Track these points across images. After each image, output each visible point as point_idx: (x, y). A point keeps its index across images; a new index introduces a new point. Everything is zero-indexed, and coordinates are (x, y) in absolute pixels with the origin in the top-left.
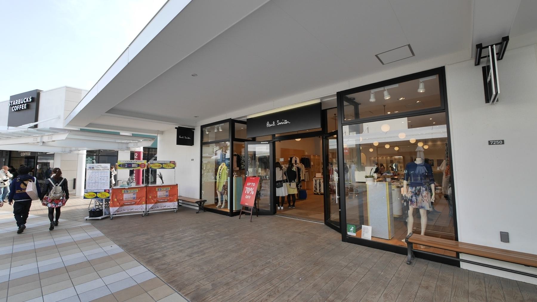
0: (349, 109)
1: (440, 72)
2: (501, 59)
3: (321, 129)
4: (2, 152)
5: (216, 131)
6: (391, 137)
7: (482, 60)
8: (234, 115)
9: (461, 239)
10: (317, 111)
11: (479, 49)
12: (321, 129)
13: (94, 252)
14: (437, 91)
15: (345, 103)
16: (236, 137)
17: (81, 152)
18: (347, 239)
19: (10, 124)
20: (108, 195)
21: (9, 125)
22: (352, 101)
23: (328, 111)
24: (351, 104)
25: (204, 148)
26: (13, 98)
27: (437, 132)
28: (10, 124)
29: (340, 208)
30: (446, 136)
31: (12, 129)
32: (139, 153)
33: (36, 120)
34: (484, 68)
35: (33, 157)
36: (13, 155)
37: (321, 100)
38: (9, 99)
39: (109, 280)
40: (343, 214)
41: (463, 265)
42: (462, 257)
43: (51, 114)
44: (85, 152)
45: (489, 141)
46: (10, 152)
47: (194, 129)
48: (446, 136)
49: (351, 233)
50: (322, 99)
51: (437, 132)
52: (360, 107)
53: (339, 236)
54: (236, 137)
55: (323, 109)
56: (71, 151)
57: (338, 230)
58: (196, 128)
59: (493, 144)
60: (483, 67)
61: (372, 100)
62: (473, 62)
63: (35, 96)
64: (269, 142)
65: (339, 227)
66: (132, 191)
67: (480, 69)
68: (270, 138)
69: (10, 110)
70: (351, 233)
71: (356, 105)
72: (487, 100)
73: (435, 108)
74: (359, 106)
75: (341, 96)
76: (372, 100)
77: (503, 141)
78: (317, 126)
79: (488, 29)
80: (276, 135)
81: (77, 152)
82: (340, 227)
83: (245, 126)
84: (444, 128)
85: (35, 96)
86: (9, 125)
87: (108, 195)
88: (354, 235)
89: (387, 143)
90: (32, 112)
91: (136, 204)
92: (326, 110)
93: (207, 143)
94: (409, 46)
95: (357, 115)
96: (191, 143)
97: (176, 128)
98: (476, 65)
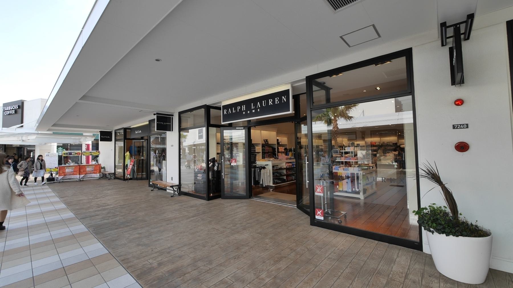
0: (319, 94)
1: (408, 54)
2: (468, 39)
4: (6, 147)
8: (209, 101)
11: (444, 28)
13: (53, 200)
14: (404, 75)
15: (315, 88)
16: (127, 137)
17: (52, 144)
18: (315, 223)
20: (57, 170)
22: (322, 86)
23: (301, 96)
24: (322, 89)
25: (116, 142)
26: (5, 105)
31: (6, 130)
32: (88, 145)
33: (22, 122)
34: (451, 50)
35: (20, 148)
38: (2, 105)
39: (63, 256)
41: (168, 191)
43: (32, 116)
44: (55, 145)
45: (453, 125)
46: (5, 145)
47: (173, 115)
49: (319, 217)
52: (331, 91)
53: (306, 219)
54: (212, 122)
56: (46, 144)
58: (174, 114)
59: (457, 128)
60: (450, 48)
63: (20, 104)
64: (244, 127)
66: (71, 168)
67: (446, 51)
69: (4, 115)
70: (319, 217)
71: (327, 90)
73: (403, 88)
74: (331, 91)
75: (311, 80)
77: (467, 125)
79: (454, 8)
81: (49, 144)
82: (309, 209)
85: (20, 104)
87: (57, 170)
90: (19, 115)
91: (73, 174)
93: (186, 130)
94: (374, 26)
96: (110, 140)
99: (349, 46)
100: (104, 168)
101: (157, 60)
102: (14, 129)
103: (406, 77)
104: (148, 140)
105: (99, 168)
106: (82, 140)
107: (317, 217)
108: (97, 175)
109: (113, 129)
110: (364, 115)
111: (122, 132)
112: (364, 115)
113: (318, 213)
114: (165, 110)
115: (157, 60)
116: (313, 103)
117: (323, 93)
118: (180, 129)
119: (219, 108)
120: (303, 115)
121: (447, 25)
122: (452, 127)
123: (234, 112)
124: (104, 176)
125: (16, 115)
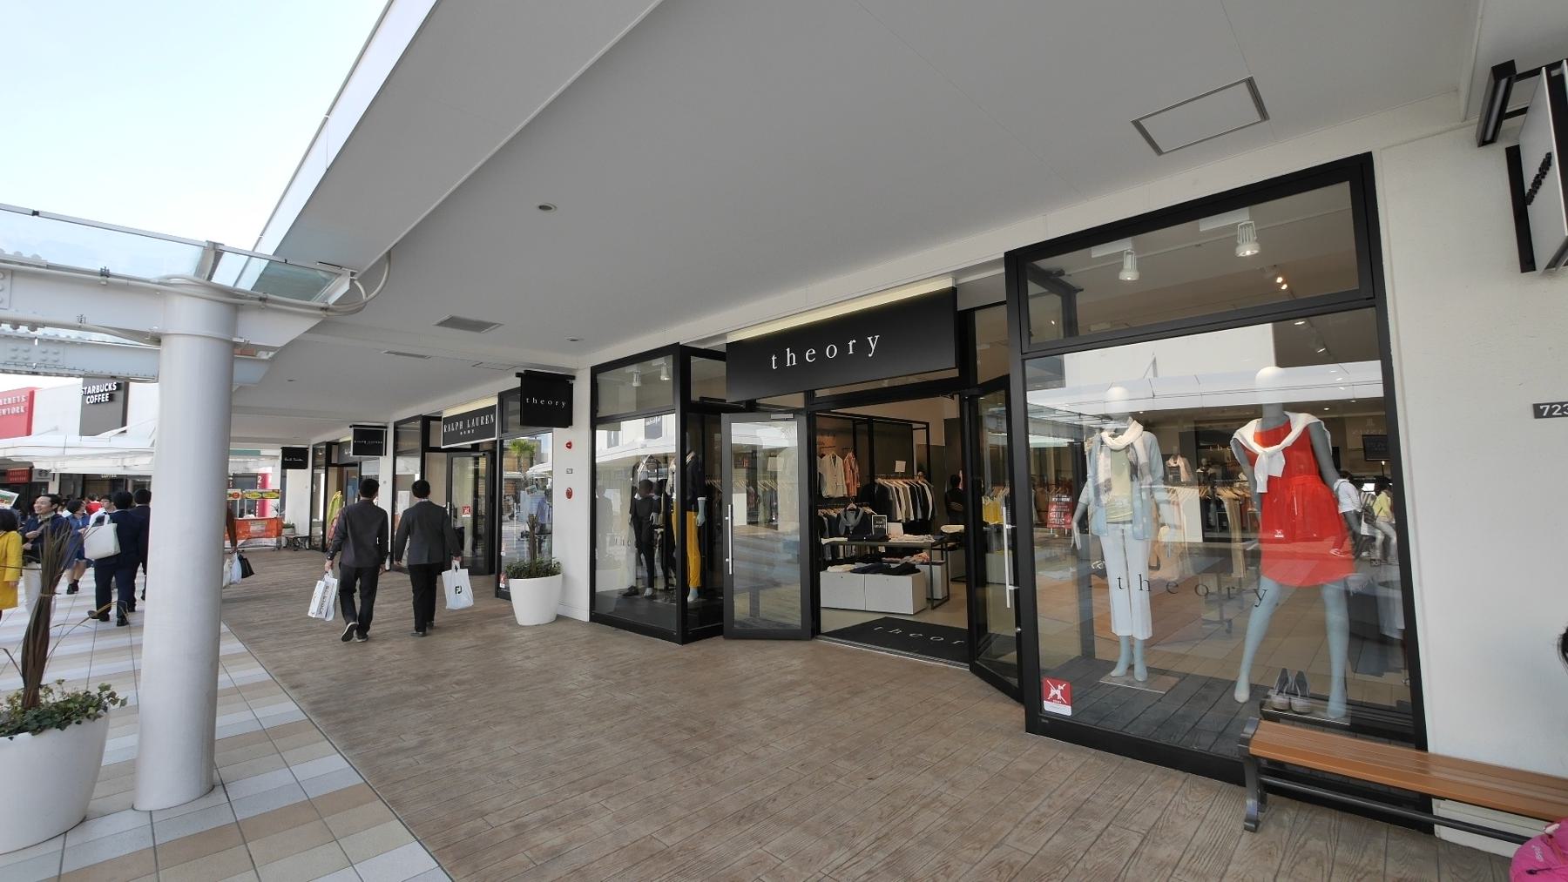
0: (1044, 309)
1: (1357, 173)
3: (955, 373)
5: (635, 384)
6: (1228, 392)
7: (1506, 123)
8: (687, 332)
9: (1435, 743)
10: (945, 315)
12: (955, 373)
15: (1033, 288)
18: (1040, 724)
19: (83, 432)
21: (82, 434)
22: (1054, 281)
23: (978, 314)
24: (1052, 291)
25: (399, 460)
27: (1354, 380)
28: (83, 432)
29: (1018, 624)
30: (1378, 391)
33: (124, 423)
36: (876, 427)
37: (955, 279)
40: (1027, 640)
41: (1442, 832)
42: (1441, 809)
47: (573, 378)
48: (1378, 391)
49: (1056, 706)
50: (957, 274)
51: (1354, 380)
52: (1080, 299)
53: (1018, 713)
55: (962, 306)
57: (1017, 695)
58: (578, 375)
59: (1550, 415)
60: (1509, 150)
61: (1129, 275)
62: (1472, 130)
65: (1014, 681)
68: (798, 400)
69: (84, 405)
70: (1056, 706)
71: (1068, 293)
72: (1523, 270)
73: (1339, 304)
75: (1019, 263)
76: (1129, 275)
78: (944, 366)
80: (819, 394)
82: (1019, 680)
83: (722, 365)
84: (1373, 369)
86: (82, 434)
88: (1066, 711)
89: (267, 349)
90: (118, 405)
92: (974, 309)
93: (612, 421)
94: (1250, 83)
95: (1070, 324)
96: (304, 466)
97: (518, 375)
98: (1483, 142)
99: (1158, 151)
100: (293, 527)
101: (541, 207)
102: (109, 440)
103: (1353, 247)
104: (493, 453)
105: (278, 526)
106: (250, 465)
107: (1048, 706)
108: (272, 542)
109: (387, 417)
110: (1155, 375)
111: (418, 424)
112: (1155, 375)
113: (1053, 692)
114: (370, 420)
115: (541, 207)
116: (1030, 335)
117: (1055, 301)
118: (596, 422)
119: (439, 419)
120: (986, 370)
121: (1519, 71)
122: (1531, 412)
123: (757, 366)
124: (294, 544)
125: (112, 405)
